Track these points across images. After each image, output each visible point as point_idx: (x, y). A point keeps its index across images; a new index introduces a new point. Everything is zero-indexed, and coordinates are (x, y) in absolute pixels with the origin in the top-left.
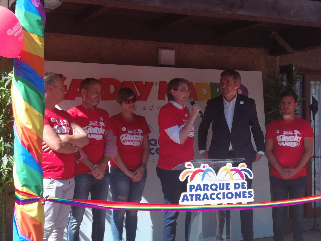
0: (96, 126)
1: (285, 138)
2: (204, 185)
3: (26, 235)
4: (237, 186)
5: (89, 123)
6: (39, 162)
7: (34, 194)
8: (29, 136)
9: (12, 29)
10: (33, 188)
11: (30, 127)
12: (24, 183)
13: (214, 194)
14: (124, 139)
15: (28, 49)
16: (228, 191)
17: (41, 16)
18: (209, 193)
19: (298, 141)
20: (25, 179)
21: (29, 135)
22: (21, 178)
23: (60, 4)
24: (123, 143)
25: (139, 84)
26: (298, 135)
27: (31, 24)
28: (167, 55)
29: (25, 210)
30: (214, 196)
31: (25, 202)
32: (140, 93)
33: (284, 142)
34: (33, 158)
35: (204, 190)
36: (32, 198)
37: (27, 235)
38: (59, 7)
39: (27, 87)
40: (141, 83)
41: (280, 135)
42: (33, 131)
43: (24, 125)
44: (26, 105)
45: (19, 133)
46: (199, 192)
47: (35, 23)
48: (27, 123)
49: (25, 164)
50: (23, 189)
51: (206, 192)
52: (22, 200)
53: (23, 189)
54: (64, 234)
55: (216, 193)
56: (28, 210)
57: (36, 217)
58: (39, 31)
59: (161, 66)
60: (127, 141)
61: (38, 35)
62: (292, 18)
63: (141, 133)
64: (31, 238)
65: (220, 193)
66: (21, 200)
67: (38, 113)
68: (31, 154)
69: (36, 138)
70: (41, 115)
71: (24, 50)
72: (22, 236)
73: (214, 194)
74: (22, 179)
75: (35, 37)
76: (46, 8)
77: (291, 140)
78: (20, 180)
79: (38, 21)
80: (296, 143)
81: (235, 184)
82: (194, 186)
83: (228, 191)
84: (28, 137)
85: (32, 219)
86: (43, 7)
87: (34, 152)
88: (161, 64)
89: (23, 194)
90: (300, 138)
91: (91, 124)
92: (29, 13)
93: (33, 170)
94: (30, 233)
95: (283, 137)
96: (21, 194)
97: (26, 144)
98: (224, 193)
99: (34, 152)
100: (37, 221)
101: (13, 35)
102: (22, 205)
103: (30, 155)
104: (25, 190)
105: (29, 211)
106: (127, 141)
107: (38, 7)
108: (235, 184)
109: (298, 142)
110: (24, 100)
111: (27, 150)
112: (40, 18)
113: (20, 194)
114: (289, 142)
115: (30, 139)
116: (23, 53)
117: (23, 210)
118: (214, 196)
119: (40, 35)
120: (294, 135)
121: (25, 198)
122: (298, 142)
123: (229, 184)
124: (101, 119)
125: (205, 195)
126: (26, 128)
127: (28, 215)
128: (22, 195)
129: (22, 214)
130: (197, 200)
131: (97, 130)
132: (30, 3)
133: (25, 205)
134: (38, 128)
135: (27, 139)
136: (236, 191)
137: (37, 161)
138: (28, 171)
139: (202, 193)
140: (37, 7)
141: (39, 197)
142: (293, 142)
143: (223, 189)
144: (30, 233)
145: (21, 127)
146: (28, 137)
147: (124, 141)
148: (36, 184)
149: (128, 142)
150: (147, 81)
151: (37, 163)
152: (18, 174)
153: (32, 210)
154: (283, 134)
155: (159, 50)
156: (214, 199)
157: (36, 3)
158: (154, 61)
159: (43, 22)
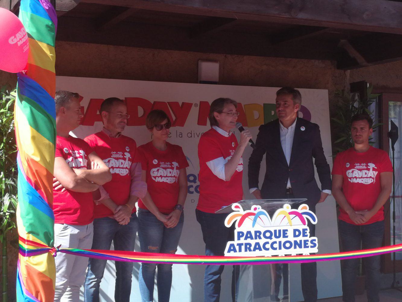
0: (120, 158)
1: (357, 173)
2: (256, 232)
4: (297, 233)
5: (355, 166)
6: (49, 203)
7: (42, 243)
8: (36, 171)
10: (42, 235)
11: (37, 159)
12: (30, 230)
13: (268, 243)
14: (156, 174)
15: (36, 61)
16: (286, 239)
17: (52, 20)
18: (262, 241)
19: (373, 177)
20: (31, 225)
21: (37, 169)
22: (27, 222)
23: (76, 5)
26: (374, 169)
27: (38, 30)
29: (31, 263)
30: (268, 246)
31: (31, 253)
33: (356, 177)
34: (41, 198)
35: (256, 238)
36: (40, 248)
37: (34, 295)
39: (34, 109)
41: (350, 169)
42: (42, 164)
43: (30, 157)
44: (32, 132)
46: (249, 241)
47: (44, 30)
48: (33, 155)
49: (31, 206)
50: (28, 237)
51: (258, 240)
52: (27, 251)
53: (28, 237)
55: (271, 241)
56: (35, 263)
57: (45, 271)
58: (49, 38)
60: (158, 177)
63: (177, 167)
64: (39, 299)
65: (275, 242)
66: (26, 250)
67: (47, 141)
69: (45, 173)
70: (51, 144)
73: (268, 243)
74: (28, 224)
75: (44, 46)
77: (365, 176)
79: (47, 26)
80: (371, 179)
81: (295, 231)
82: (243, 233)
83: (286, 239)
84: (34, 171)
85: (40, 274)
87: (43, 190)
89: (29, 243)
90: (376, 173)
91: (114, 156)
92: (37, 17)
93: (41, 213)
94: (37, 293)
95: (355, 172)
96: (26, 243)
97: (33, 180)
98: (280, 242)
99: (43, 190)
100: (46, 277)
102: (28, 257)
103: (37, 194)
104: (31, 238)
105: (36, 265)
107: (48, 8)
108: (295, 231)
109: (373, 178)
111: (34, 188)
112: (50, 23)
113: (25, 243)
114: (362, 178)
116: (28, 67)
117: (29, 264)
118: (268, 246)
119: (50, 43)
120: (369, 170)
121: (31, 248)
122: (373, 178)
123: (287, 230)
124: (126, 149)
125: (257, 244)
126: (32, 160)
128: (27, 244)
129: (28, 268)
130: (247, 251)
131: (122, 163)
133: (32, 257)
135: (33, 174)
136: (296, 239)
137: (46, 202)
138: (36, 215)
139: (253, 242)
141: (49, 247)
142: (367, 178)
143: (279, 237)
144: (37, 293)
145: (26, 159)
146: (34, 171)
147: (155, 177)
148: (45, 231)
152: (23, 217)
153: (40, 263)
156: (268, 249)
157: (44, 4)
159: (54, 27)
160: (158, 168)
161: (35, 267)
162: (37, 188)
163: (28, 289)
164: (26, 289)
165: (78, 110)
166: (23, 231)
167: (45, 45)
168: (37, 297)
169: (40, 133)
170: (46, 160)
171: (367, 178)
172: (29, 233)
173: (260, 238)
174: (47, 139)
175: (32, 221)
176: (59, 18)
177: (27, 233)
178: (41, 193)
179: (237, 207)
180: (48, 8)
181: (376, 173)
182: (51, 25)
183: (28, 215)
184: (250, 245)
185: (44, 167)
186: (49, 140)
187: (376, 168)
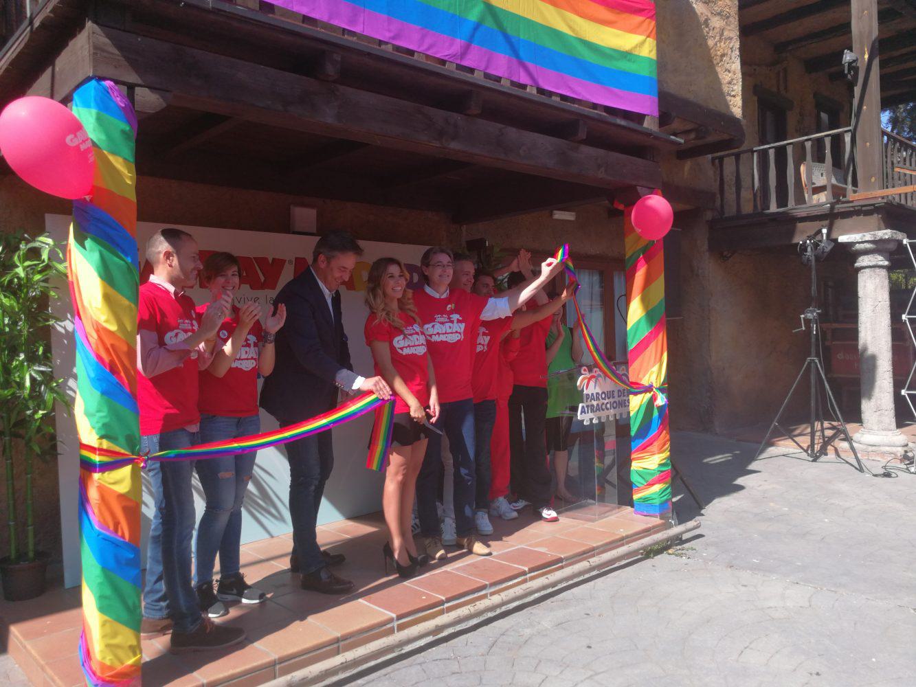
1: (438, 328)
3: (109, 527)
5: (435, 319)
6: (132, 393)
7: (122, 451)
8: (112, 345)
9: (76, 136)
10: (122, 440)
11: (113, 327)
12: (103, 432)
14: (402, 344)
15: (107, 183)
17: (129, 122)
19: (459, 331)
20: (105, 425)
21: (112, 342)
22: (97, 422)
23: (164, 105)
24: (400, 351)
25: (262, 261)
26: (459, 321)
27: (110, 138)
28: (305, 215)
29: (106, 482)
31: (105, 467)
32: (264, 275)
33: (438, 334)
34: (121, 386)
36: (120, 458)
37: (112, 528)
38: (163, 110)
39: (105, 252)
40: (265, 259)
42: (119, 334)
43: (100, 324)
44: (104, 288)
45: (91, 339)
47: (117, 135)
48: (106, 321)
49: (105, 397)
50: (101, 444)
52: (99, 464)
53: (101, 444)
54: (143, 481)
55: (606, 402)
56: (112, 481)
57: (128, 492)
58: (128, 150)
59: (294, 233)
60: (406, 347)
61: (125, 160)
62: (755, 70)
64: (120, 533)
66: (98, 463)
67: (126, 302)
68: (117, 377)
69: (125, 348)
70: (133, 306)
71: (97, 183)
72: (101, 530)
74: (99, 425)
75: (118, 163)
76: (138, 109)
77: (449, 331)
78: (94, 428)
79: (123, 132)
81: (619, 391)
84: (109, 346)
85: (121, 497)
86: (132, 107)
87: (122, 374)
88: (296, 230)
89: (102, 452)
90: (463, 326)
92: (106, 116)
93: (119, 407)
94: (117, 524)
95: (436, 327)
96: (98, 453)
97: (107, 359)
99: (122, 374)
100: (130, 500)
101: (78, 147)
102: (100, 474)
103: (114, 379)
104: (105, 444)
105: (114, 483)
106: (406, 347)
107: (124, 106)
110: (101, 277)
111: (108, 371)
112: (127, 128)
113: (95, 453)
114: (446, 333)
115: (114, 350)
116: (93, 190)
117: (103, 483)
119: (127, 157)
121: (105, 459)
122: (460, 333)
126: (106, 330)
127: (111, 490)
128: (99, 455)
129: (101, 489)
132: (108, 98)
133: (106, 473)
134: (127, 330)
135: (107, 350)
137: (127, 391)
138: (113, 412)
139: (595, 403)
140: (123, 108)
141: (133, 455)
142: (452, 333)
144: (117, 524)
145: (95, 327)
146: (109, 346)
147: (402, 349)
148: (129, 433)
149: (408, 348)
150: (277, 257)
151: (453, 519)
152: (87, 414)
153: (120, 481)
154: (434, 321)
155: (292, 207)
157: (118, 99)
158: (284, 226)
159: (133, 134)
160: (176, 331)
161: (112, 487)
162: (113, 370)
163: (102, 520)
164: (99, 521)
165: (194, 257)
166: (88, 433)
167: (121, 160)
168: (116, 531)
169: (116, 290)
170: (126, 328)
171: (452, 333)
172: (102, 437)
173: (599, 400)
174: (126, 298)
175: (106, 420)
176: (139, 123)
177: (98, 437)
178: (120, 378)
179: (585, 370)
180: (124, 106)
181: (463, 326)
182: (129, 130)
183: (98, 411)
184: (593, 405)
185: (123, 337)
186: (128, 299)
187: (460, 318)
